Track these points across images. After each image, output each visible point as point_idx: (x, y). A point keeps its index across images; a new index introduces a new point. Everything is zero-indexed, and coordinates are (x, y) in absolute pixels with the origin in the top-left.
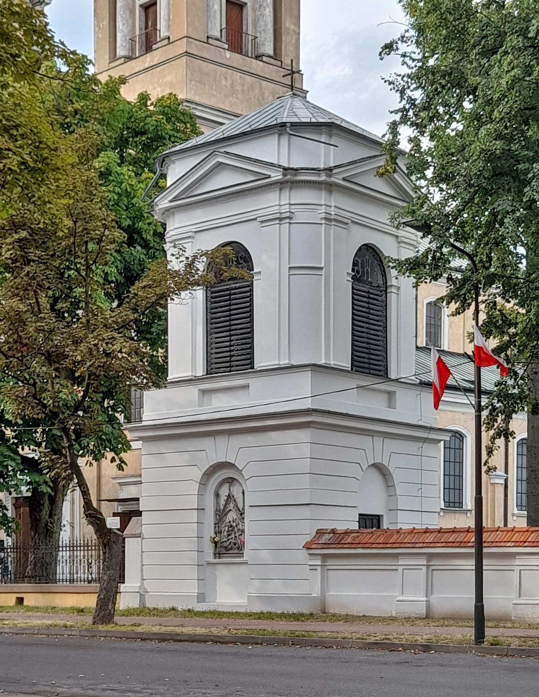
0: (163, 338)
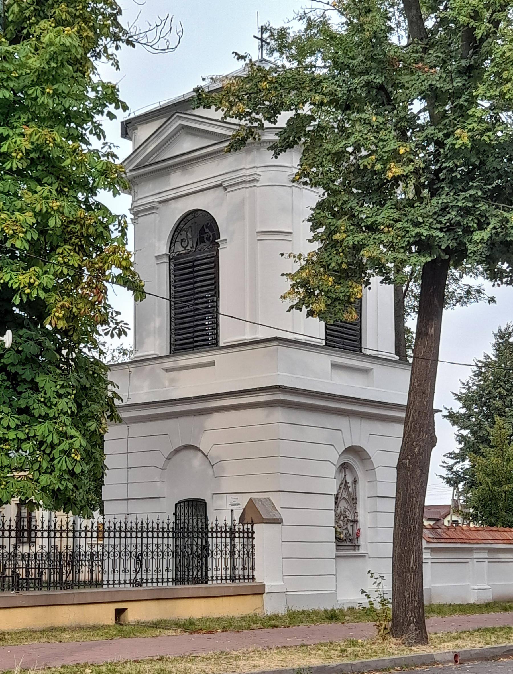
0: (496, 270)
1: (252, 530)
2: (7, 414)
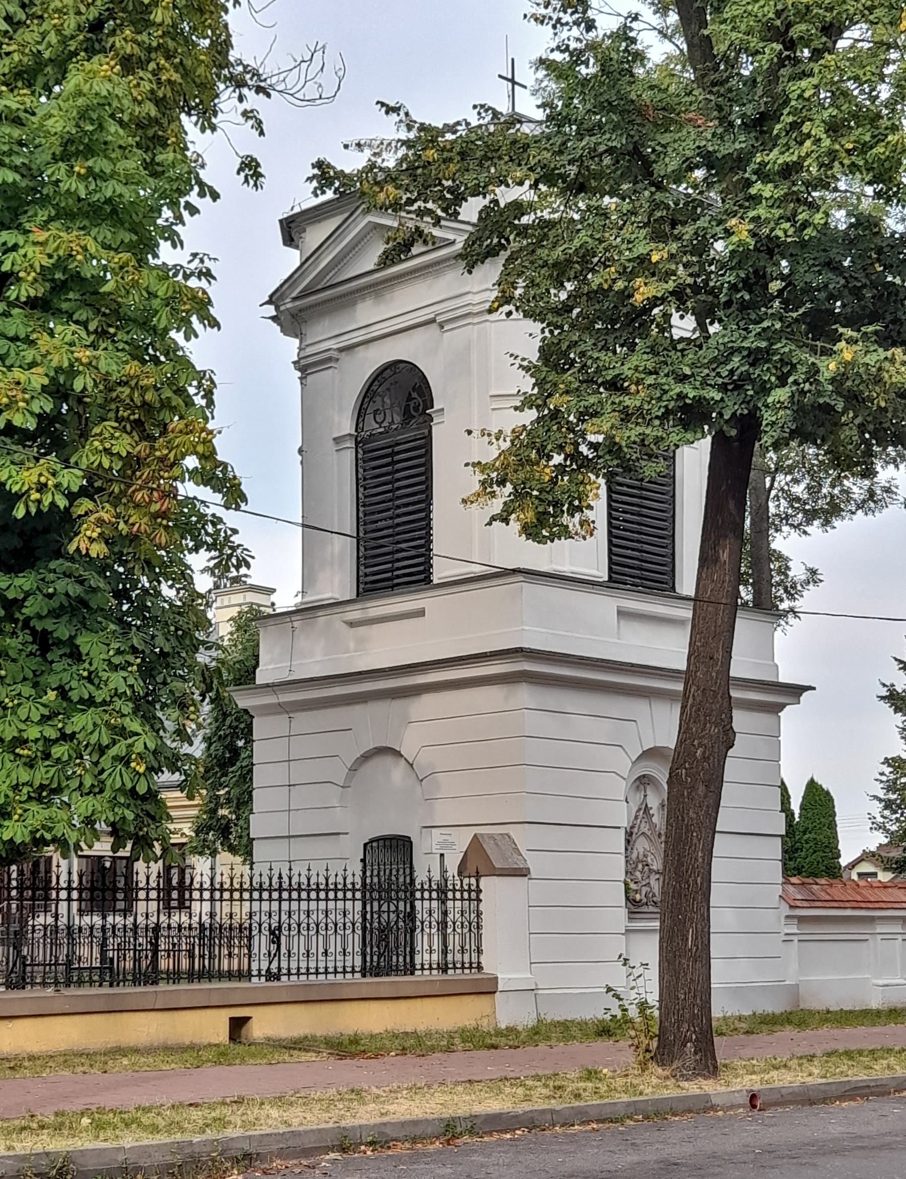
1: (478, 886)
2: (28, 699)
